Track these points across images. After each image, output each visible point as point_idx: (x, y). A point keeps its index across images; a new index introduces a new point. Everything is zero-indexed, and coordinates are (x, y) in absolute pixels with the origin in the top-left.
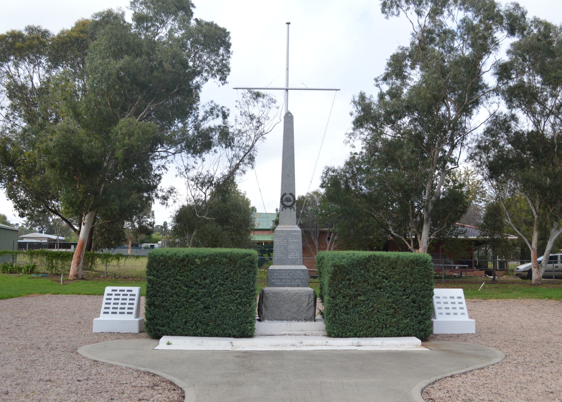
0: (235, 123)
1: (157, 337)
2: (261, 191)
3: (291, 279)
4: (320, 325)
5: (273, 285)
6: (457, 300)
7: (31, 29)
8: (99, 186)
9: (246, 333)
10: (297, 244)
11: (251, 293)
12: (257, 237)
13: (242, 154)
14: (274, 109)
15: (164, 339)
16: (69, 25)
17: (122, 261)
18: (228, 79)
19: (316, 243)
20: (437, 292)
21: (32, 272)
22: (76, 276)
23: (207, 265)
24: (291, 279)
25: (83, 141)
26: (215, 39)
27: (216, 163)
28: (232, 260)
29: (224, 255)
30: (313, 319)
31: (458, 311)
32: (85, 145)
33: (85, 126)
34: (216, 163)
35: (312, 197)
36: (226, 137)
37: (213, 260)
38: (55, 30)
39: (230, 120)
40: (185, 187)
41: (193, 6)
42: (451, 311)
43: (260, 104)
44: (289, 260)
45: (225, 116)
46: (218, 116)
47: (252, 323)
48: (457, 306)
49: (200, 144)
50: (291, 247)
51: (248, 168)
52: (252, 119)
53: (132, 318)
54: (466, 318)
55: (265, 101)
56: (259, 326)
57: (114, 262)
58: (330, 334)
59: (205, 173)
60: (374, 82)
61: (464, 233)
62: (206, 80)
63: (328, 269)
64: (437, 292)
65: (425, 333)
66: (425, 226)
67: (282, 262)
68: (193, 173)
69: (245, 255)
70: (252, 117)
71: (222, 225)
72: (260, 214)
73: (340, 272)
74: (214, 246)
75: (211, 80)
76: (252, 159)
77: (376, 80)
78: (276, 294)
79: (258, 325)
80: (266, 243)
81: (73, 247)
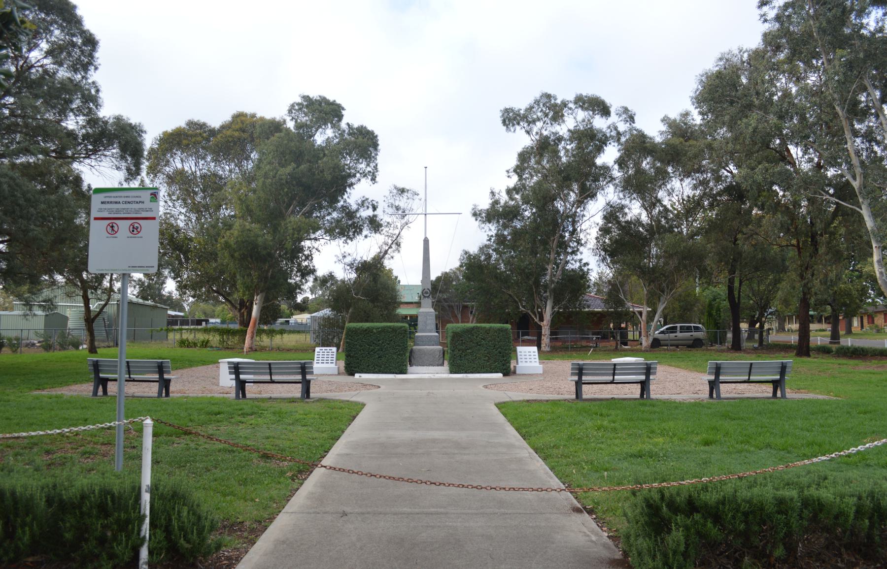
0: (383, 216)
1: (353, 375)
2: (406, 271)
3: (429, 341)
4: (446, 367)
5: (418, 345)
6: (532, 354)
7: (191, 124)
8: (268, 271)
9: (404, 372)
10: (432, 322)
11: (405, 348)
12: (403, 311)
13: (390, 242)
14: (417, 201)
15: (357, 375)
16: (227, 117)
17: (285, 336)
18: (377, 179)
19: (459, 316)
20: (520, 349)
21: (206, 347)
22: (251, 348)
23: (379, 333)
24: (429, 341)
25: (258, 236)
26: (364, 143)
27: (365, 247)
28: (394, 330)
29: (390, 327)
30: (442, 365)
31: (533, 360)
32: (260, 239)
33: (258, 221)
34: (365, 247)
35: (454, 273)
36: (375, 225)
37: (384, 330)
38: (215, 122)
39: (379, 212)
40: (342, 271)
41: (343, 109)
42: (528, 360)
43: (405, 197)
44: (427, 330)
45: (375, 208)
46: (368, 208)
47: (406, 366)
48: (532, 357)
49: (348, 227)
50: (429, 322)
51: (396, 254)
52: (397, 210)
53: (333, 365)
54: (537, 364)
55: (409, 195)
56: (410, 369)
57: (278, 336)
58: (451, 373)
59: (359, 259)
60: (506, 174)
61: (589, 307)
62: (359, 180)
63: (450, 334)
64: (520, 349)
65: (507, 372)
66: (548, 303)
67: (423, 331)
68: (348, 260)
69: (401, 327)
70: (398, 208)
71: (373, 301)
72: (405, 286)
73: (457, 336)
74: (367, 321)
75: (363, 180)
76: (398, 245)
77: (508, 172)
78: (420, 350)
79: (409, 367)
80: (411, 316)
81: (204, 323)
